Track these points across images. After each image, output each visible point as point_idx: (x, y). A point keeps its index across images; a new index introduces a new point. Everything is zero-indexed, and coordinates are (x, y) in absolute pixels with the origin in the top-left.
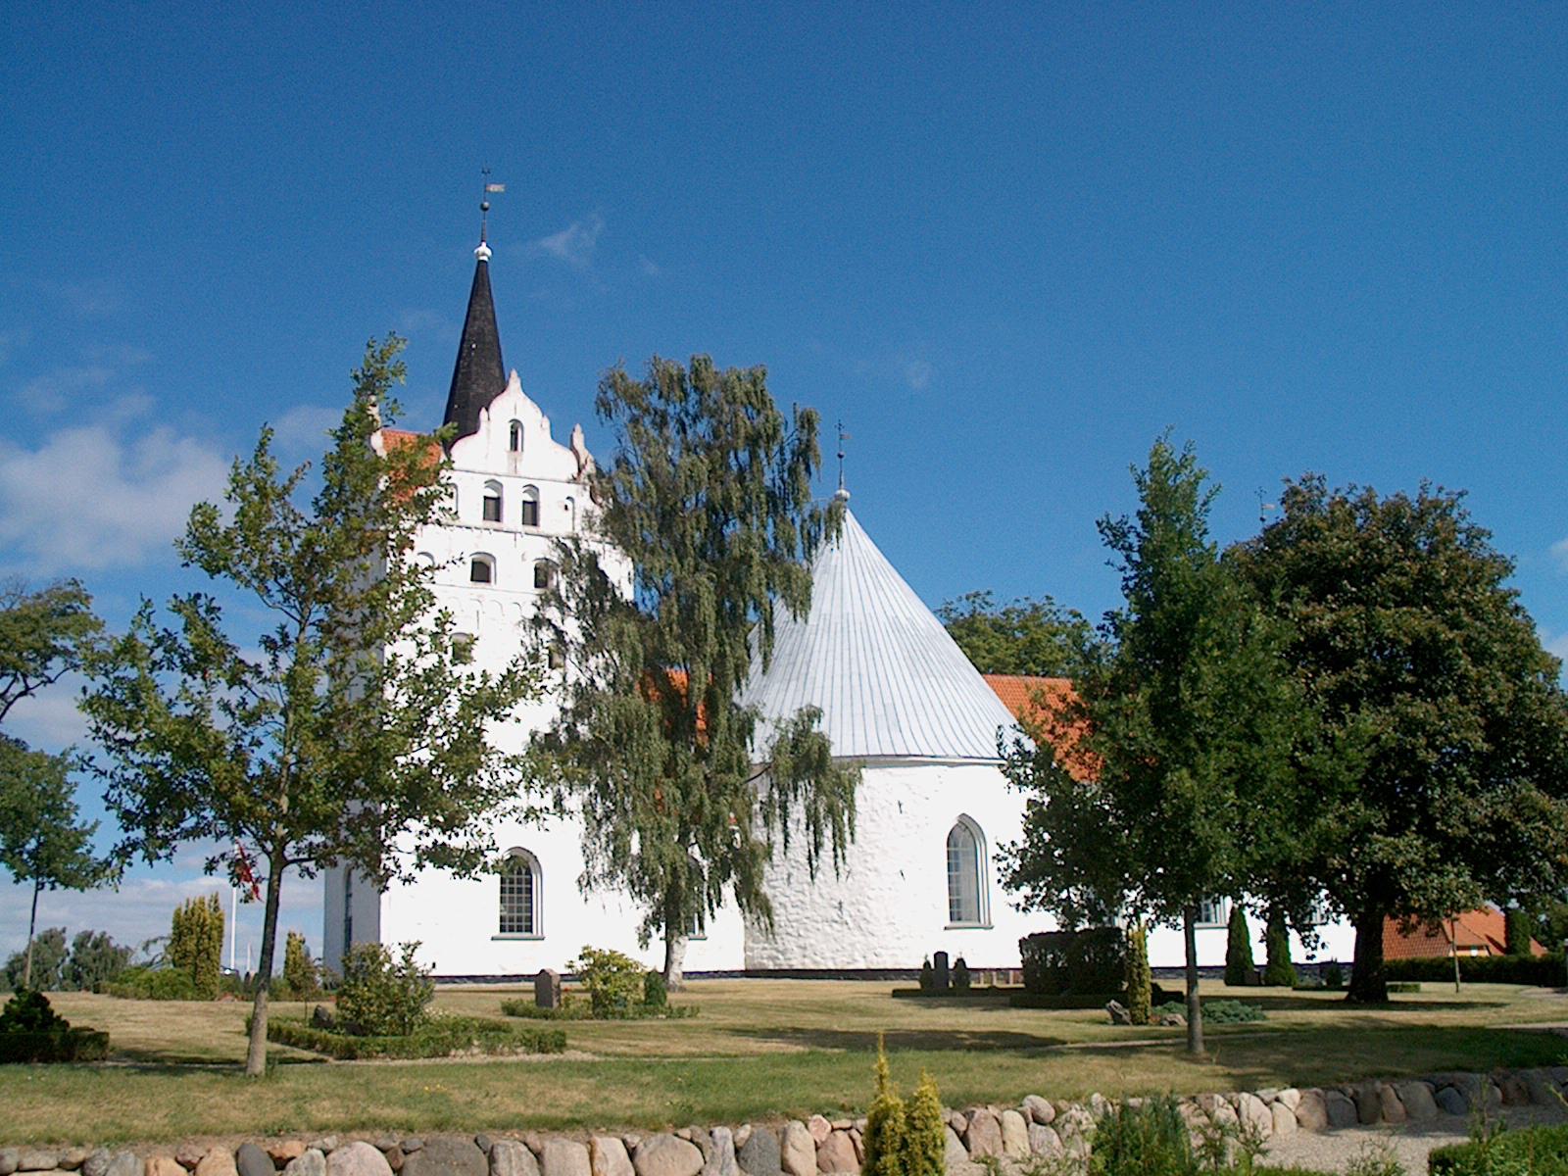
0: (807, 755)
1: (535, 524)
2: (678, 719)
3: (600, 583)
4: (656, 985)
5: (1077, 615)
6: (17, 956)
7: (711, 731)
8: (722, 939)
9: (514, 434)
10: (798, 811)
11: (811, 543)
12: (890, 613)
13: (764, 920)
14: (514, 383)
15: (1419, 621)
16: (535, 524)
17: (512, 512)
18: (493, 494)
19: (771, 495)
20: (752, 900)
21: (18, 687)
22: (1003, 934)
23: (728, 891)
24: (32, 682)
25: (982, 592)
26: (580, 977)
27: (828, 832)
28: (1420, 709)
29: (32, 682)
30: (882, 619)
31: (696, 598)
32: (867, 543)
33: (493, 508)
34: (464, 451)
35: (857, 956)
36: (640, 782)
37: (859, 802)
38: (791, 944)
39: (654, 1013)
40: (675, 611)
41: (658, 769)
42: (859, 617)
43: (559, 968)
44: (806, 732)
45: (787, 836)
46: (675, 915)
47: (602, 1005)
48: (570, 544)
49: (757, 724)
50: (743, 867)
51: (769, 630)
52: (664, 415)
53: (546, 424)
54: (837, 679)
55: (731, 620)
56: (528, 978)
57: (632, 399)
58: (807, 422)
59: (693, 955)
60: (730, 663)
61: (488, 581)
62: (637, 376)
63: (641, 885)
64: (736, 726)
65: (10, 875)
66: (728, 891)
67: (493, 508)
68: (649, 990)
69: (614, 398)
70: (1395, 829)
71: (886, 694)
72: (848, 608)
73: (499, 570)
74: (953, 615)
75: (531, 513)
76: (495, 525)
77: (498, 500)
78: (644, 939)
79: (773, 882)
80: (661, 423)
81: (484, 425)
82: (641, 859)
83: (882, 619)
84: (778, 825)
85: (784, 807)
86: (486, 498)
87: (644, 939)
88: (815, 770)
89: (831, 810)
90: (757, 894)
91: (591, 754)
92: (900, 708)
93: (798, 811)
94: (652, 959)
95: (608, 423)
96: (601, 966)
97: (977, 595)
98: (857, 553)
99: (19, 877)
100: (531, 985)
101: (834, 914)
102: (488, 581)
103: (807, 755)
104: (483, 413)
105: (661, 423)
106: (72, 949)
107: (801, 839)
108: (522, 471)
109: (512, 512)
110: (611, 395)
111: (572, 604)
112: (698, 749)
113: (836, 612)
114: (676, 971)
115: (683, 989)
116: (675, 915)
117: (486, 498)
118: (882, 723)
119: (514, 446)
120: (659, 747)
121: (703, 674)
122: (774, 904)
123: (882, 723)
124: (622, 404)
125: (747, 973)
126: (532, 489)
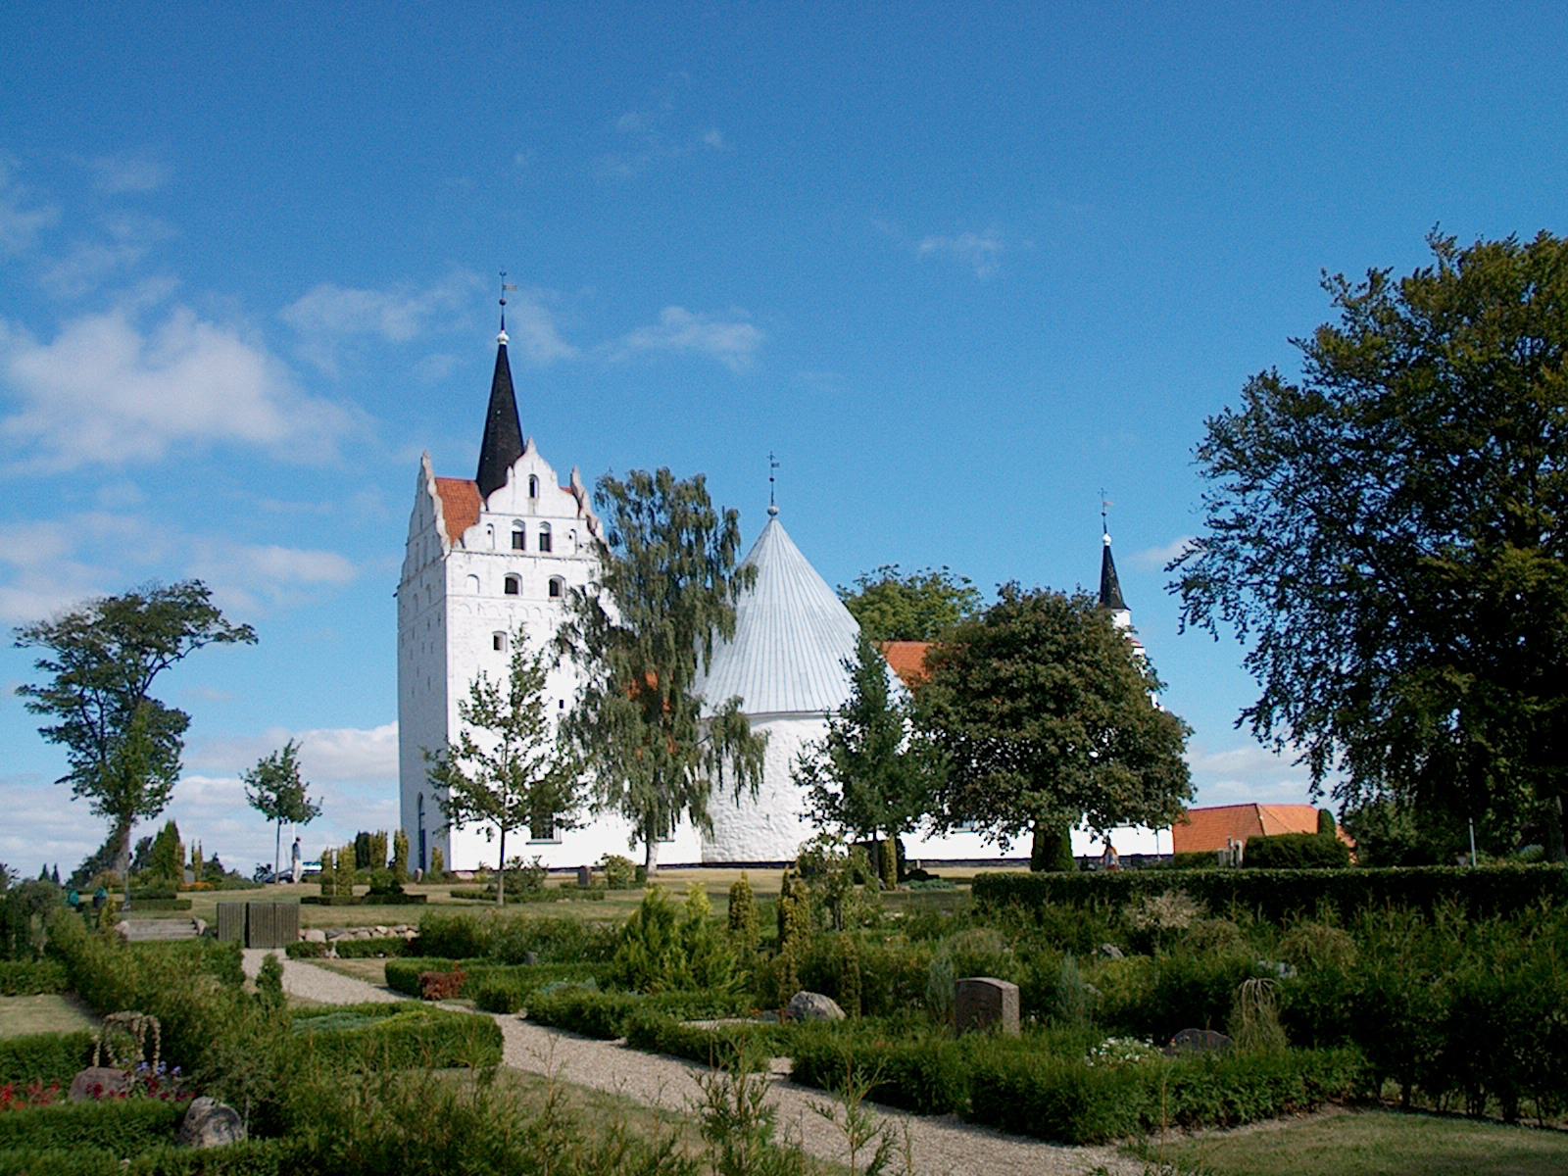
0: (733, 728)
1: (549, 550)
2: (651, 704)
3: (600, 616)
4: (641, 871)
5: (967, 581)
6: (90, 858)
7: (673, 712)
8: (684, 843)
9: (532, 485)
10: (728, 763)
11: (736, 591)
12: (807, 603)
13: (709, 831)
14: (531, 449)
15: (1059, 672)
16: (549, 550)
17: (532, 542)
18: (519, 529)
19: (709, 561)
20: (699, 816)
21: (159, 662)
22: (844, 842)
23: (685, 813)
24: (167, 657)
25: (892, 565)
26: (602, 868)
27: (748, 778)
28: (1054, 723)
29: (167, 657)
30: (800, 607)
31: (665, 634)
32: (791, 548)
33: (519, 540)
34: (497, 499)
35: (779, 852)
36: (629, 750)
37: (766, 760)
38: (734, 844)
39: (640, 887)
40: (650, 643)
41: (640, 742)
42: (784, 607)
43: (590, 864)
44: (734, 712)
45: (721, 777)
46: (652, 828)
47: (614, 883)
48: (579, 590)
49: (702, 706)
50: (695, 800)
51: (709, 649)
52: (639, 504)
53: (555, 477)
54: (767, 655)
55: (685, 643)
56: (572, 869)
57: (620, 495)
58: (731, 517)
59: (664, 853)
60: (684, 673)
61: (516, 592)
62: (622, 478)
63: (631, 809)
64: (689, 709)
65: (265, 816)
66: (685, 813)
67: (519, 540)
68: (637, 874)
69: (608, 490)
70: (1034, 788)
71: (801, 665)
72: (775, 600)
73: (524, 585)
74: (869, 584)
75: (546, 542)
76: (520, 552)
77: (522, 534)
78: (633, 844)
79: (712, 807)
80: (638, 510)
81: (510, 480)
82: (629, 795)
83: (800, 607)
84: (716, 773)
85: (719, 761)
86: (514, 533)
87: (633, 844)
88: (738, 734)
89: (748, 763)
90: (704, 815)
91: (600, 730)
92: (811, 676)
93: (728, 763)
94: (638, 857)
95: (601, 510)
96: (613, 863)
97: (887, 567)
98: (783, 556)
99: (270, 818)
100: (575, 874)
101: (764, 823)
102: (516, 592)
103: (733, 728)
104: (510, 470)
105: (638, 510)
106: (134, 853)
107: (730, 780)
108: (539, 512)
109: (532, 542)
110: (604, 491)
111: (582, 630)
112: (665, 723)
113: (767, 602)
114: (653, 864)
115: (657, 876)
116: (652, 828)
117: (514, 533)
118: (798, 687)
119: (532, 494)
120: (641, 728)
121: (667, 680)
122: (714, 819)
123: (798, 687)
124: (611, 497)
125: (703, 865)
126: (546, 525)
